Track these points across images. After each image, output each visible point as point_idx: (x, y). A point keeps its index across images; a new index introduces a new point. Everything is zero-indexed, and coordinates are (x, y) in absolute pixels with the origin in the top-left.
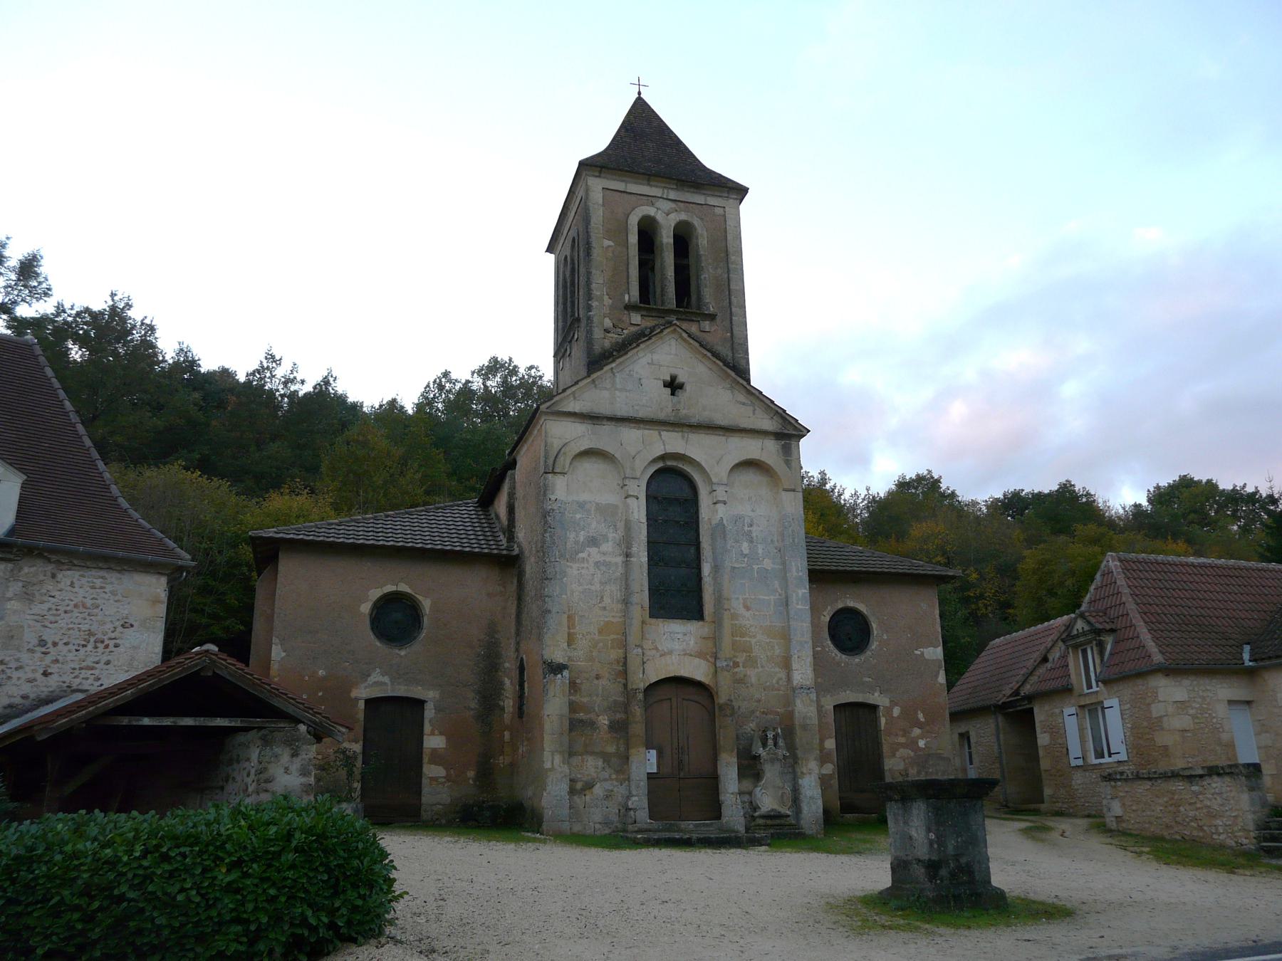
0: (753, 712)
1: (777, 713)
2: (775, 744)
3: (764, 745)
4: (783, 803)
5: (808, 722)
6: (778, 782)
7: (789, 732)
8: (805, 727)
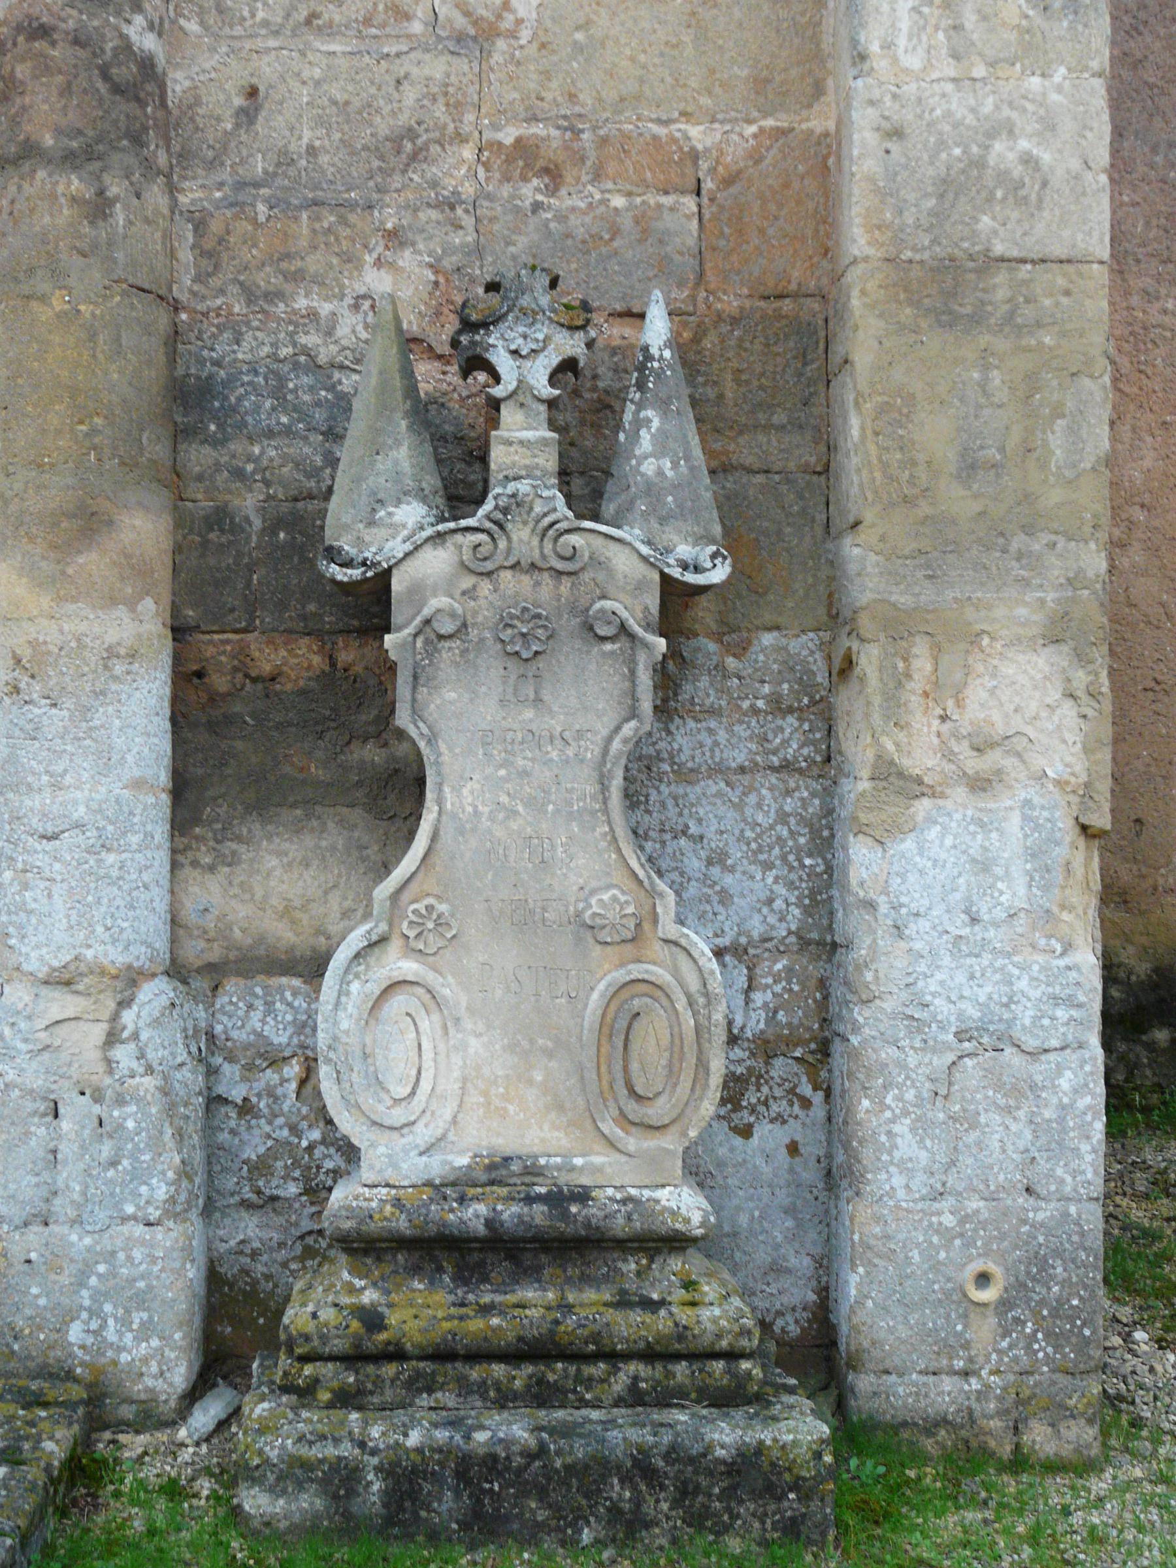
0: (408, 148)
1: (683, 171)
2: (588, 478)
3: (461, 479)
4: (616, 1084)
5: (998, 232)
6: (591, 869)
7: (772, 375)
8: (949, 288)
